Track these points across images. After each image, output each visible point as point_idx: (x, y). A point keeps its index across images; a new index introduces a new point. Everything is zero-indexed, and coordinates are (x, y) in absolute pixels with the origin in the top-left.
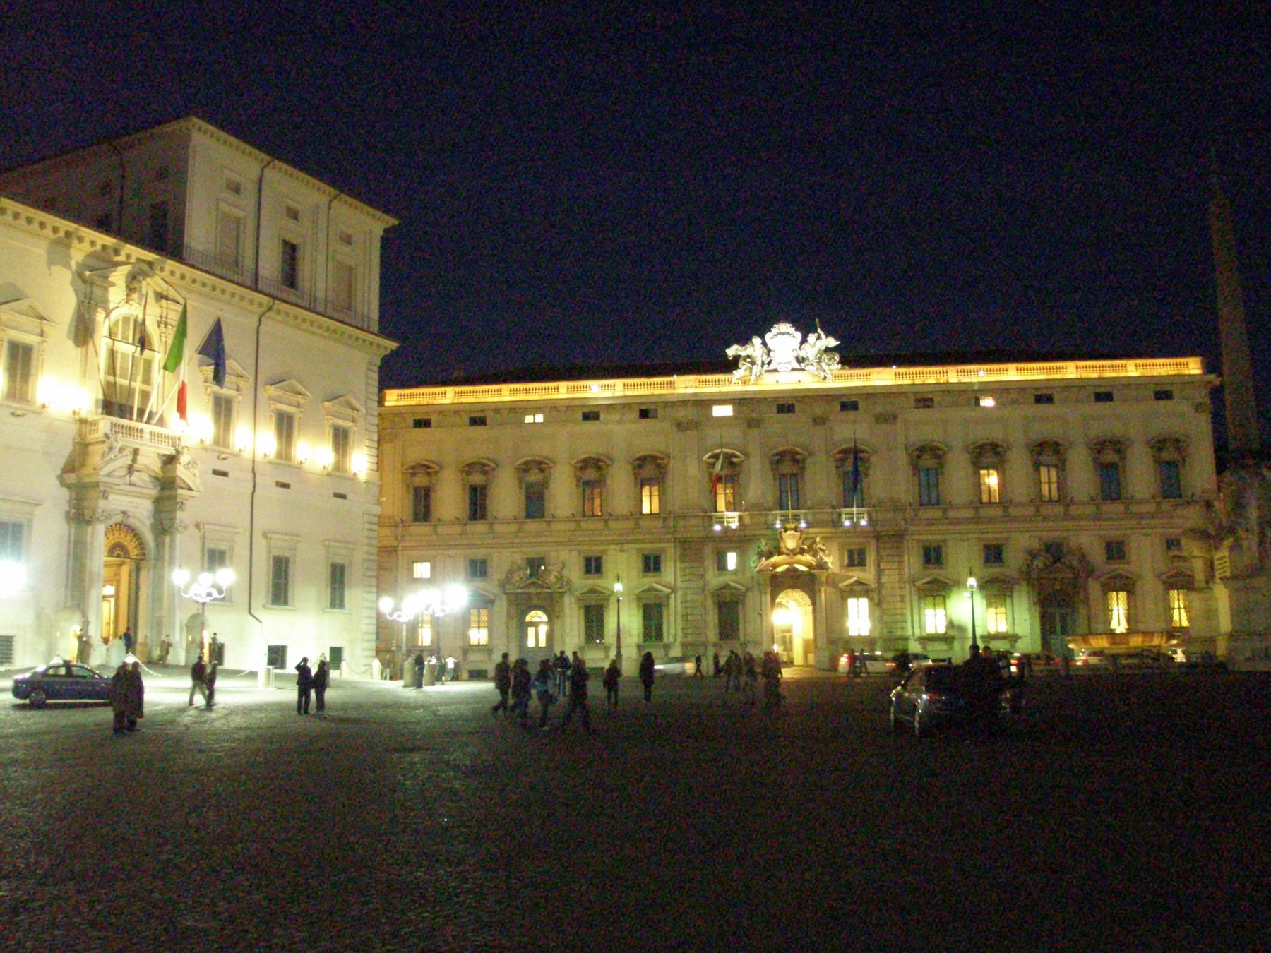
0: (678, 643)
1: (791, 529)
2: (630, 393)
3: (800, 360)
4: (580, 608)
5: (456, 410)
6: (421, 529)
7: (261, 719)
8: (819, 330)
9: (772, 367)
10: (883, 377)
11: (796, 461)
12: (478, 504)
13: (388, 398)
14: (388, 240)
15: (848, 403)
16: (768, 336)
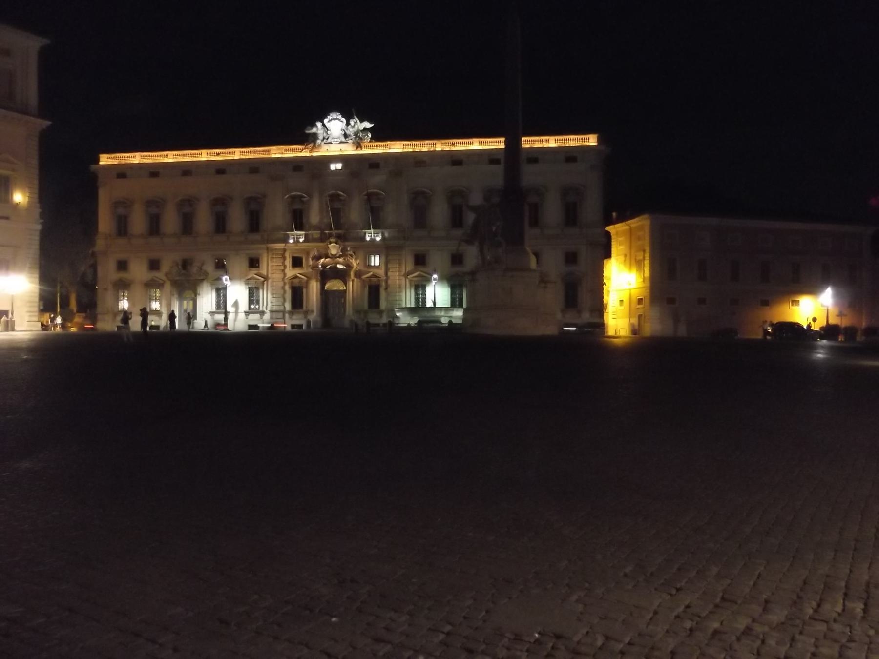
0: (268, 311)
1: (333, 242)
2: (243, 157)
3: (346, 136)
4: (246, 288)
5: (141, 166)
6: (122, 241)
7: (457, 311)
8: (355, 117)
9: (329, 141)
10: (397, 147)
11: (302, 202)
12: (154, 227)
13: (101, 159)
14: (43, 54)
15: (373, 163)
16: (326, 121)
